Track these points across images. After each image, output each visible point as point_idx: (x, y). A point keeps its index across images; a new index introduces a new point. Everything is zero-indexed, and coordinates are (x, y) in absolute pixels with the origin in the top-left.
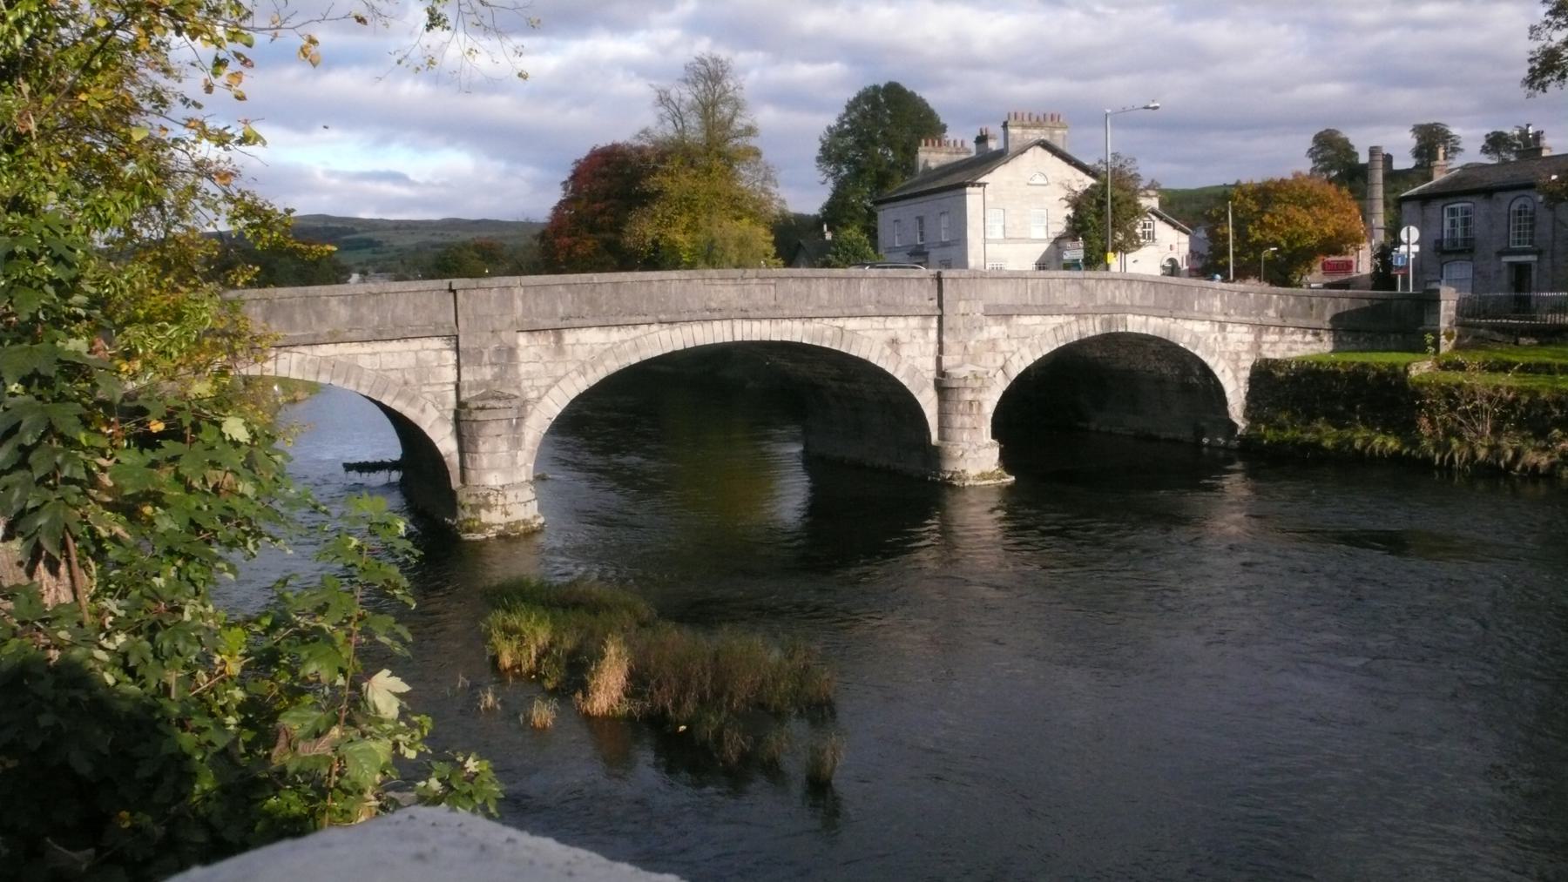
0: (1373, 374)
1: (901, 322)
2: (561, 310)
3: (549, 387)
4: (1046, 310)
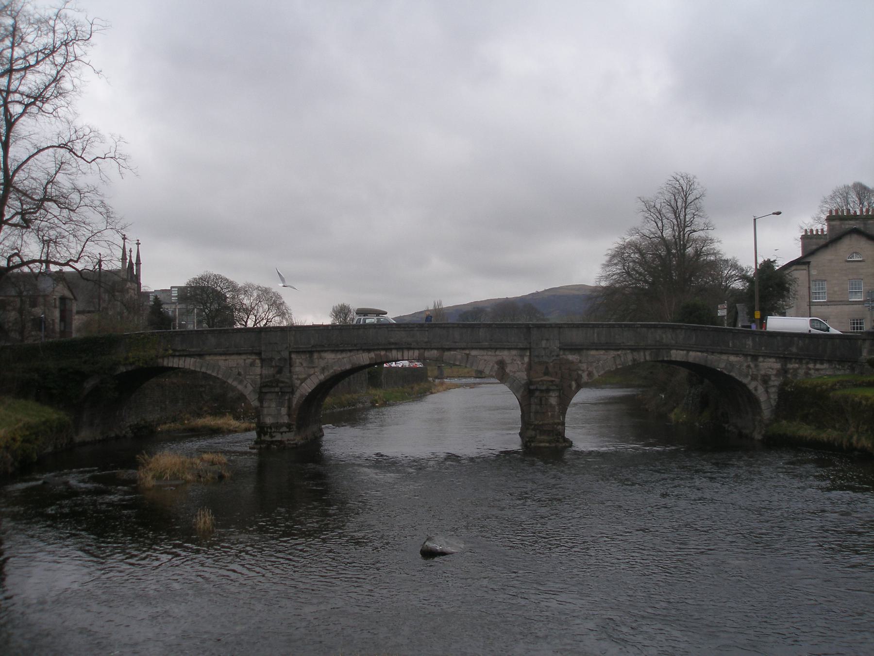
0: (175, 293)
1: (506, 353)
2: (312, 342)
3: (305, 379)
4: (607, 347)
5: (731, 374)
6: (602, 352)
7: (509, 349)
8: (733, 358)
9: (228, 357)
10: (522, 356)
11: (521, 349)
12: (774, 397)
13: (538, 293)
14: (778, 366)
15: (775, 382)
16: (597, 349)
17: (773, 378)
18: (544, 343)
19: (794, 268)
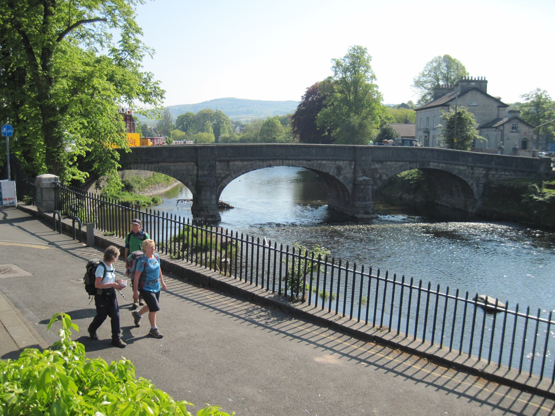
5: (461, 176)
6: (394, 163)
7: (343, 160)
8: (461, 168)
9: (176, 164)
10: (350, 165)
11: (350, 160)
12: (481, 189)
13: (206, 102)
14: (484, 172)
15: (483, 181)
16: (391, 161)
17: (481, 179)
18: (363, 158)
19: (440, 108)
